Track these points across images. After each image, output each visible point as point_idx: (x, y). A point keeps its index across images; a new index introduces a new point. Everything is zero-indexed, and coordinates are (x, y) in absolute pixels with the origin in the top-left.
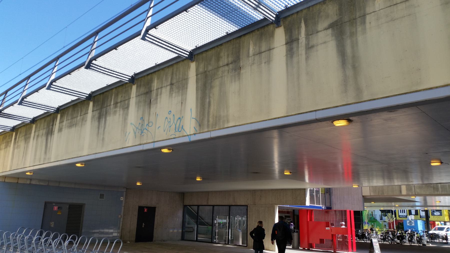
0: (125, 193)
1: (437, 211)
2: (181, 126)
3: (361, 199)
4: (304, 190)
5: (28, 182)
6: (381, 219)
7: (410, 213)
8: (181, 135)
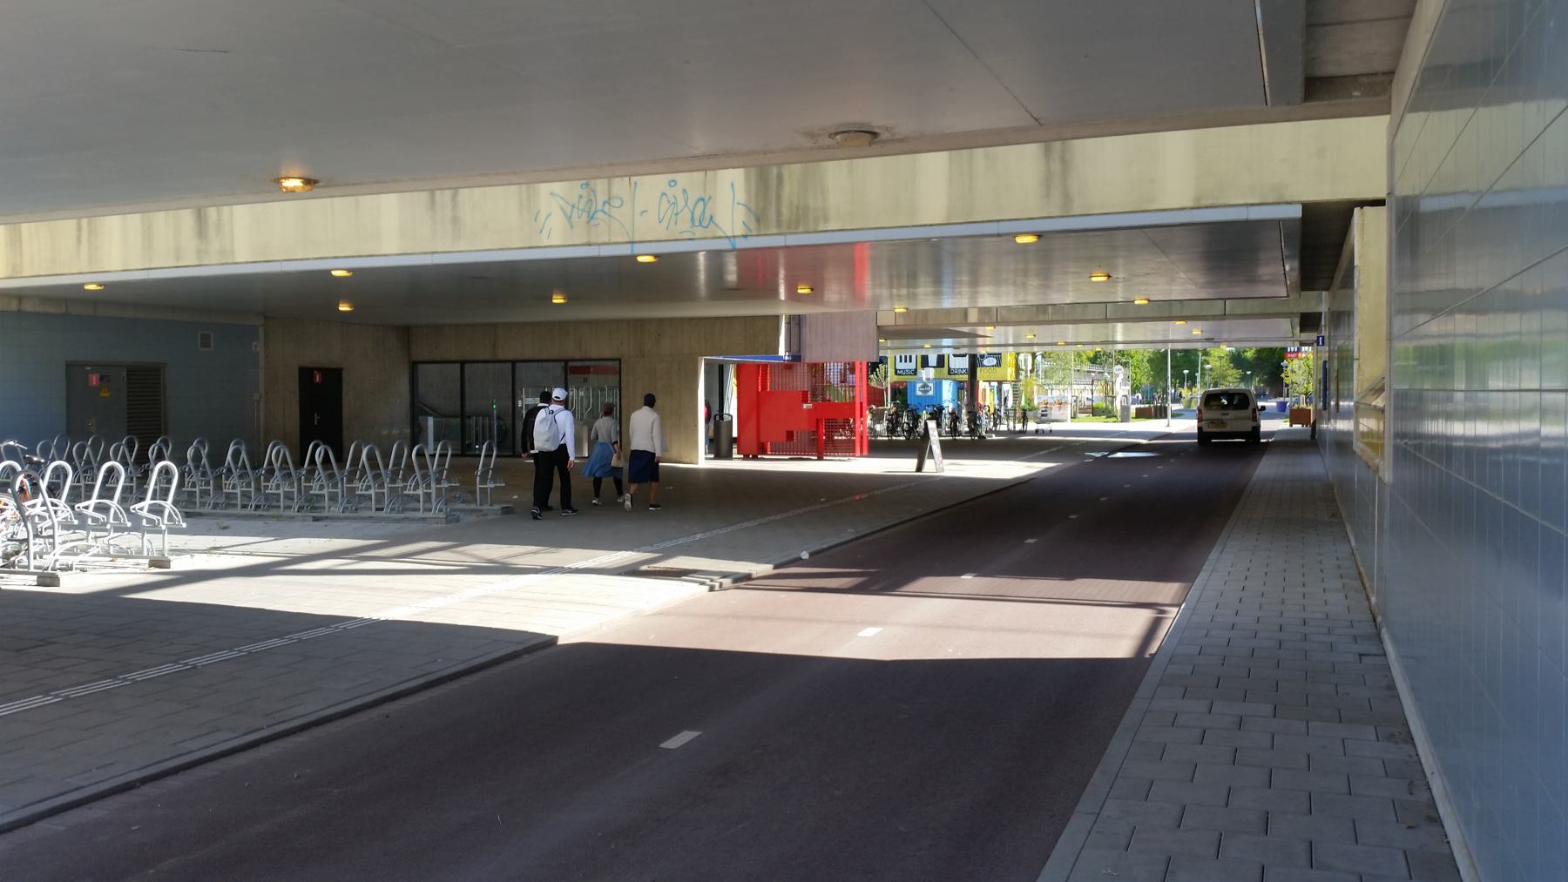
0: (261, 331)
1: (990, 355)
2: (707, 216)
3: (873, 332)
4: (777, 318)
5: (14, 306)
6: (844, 381)
7: (925, 362)
8: (709, 235)
